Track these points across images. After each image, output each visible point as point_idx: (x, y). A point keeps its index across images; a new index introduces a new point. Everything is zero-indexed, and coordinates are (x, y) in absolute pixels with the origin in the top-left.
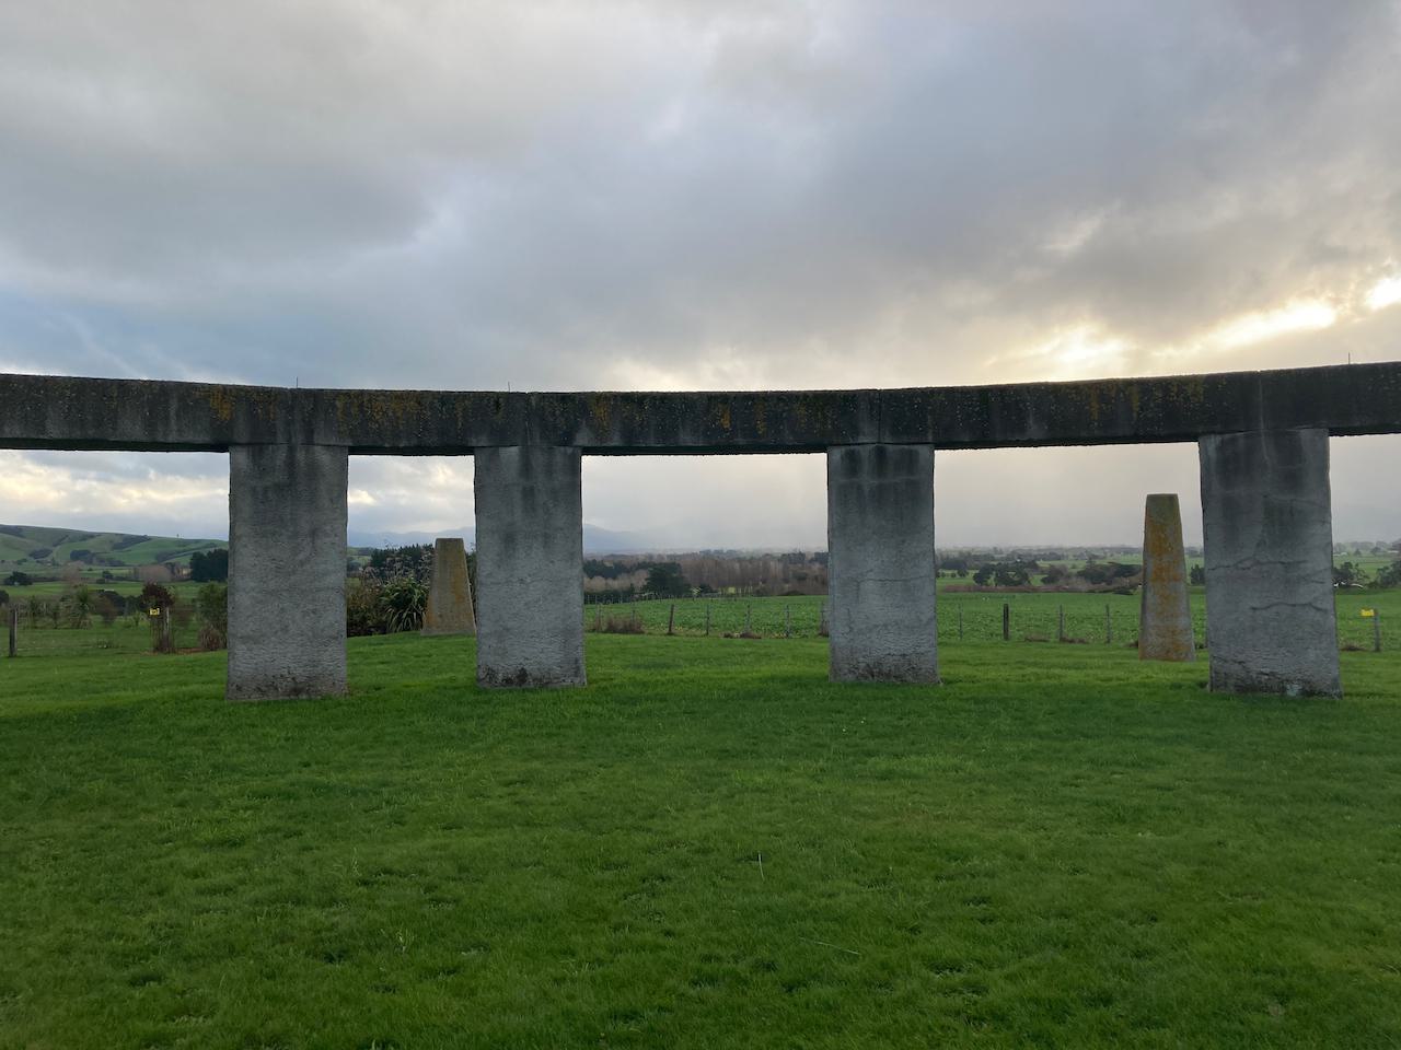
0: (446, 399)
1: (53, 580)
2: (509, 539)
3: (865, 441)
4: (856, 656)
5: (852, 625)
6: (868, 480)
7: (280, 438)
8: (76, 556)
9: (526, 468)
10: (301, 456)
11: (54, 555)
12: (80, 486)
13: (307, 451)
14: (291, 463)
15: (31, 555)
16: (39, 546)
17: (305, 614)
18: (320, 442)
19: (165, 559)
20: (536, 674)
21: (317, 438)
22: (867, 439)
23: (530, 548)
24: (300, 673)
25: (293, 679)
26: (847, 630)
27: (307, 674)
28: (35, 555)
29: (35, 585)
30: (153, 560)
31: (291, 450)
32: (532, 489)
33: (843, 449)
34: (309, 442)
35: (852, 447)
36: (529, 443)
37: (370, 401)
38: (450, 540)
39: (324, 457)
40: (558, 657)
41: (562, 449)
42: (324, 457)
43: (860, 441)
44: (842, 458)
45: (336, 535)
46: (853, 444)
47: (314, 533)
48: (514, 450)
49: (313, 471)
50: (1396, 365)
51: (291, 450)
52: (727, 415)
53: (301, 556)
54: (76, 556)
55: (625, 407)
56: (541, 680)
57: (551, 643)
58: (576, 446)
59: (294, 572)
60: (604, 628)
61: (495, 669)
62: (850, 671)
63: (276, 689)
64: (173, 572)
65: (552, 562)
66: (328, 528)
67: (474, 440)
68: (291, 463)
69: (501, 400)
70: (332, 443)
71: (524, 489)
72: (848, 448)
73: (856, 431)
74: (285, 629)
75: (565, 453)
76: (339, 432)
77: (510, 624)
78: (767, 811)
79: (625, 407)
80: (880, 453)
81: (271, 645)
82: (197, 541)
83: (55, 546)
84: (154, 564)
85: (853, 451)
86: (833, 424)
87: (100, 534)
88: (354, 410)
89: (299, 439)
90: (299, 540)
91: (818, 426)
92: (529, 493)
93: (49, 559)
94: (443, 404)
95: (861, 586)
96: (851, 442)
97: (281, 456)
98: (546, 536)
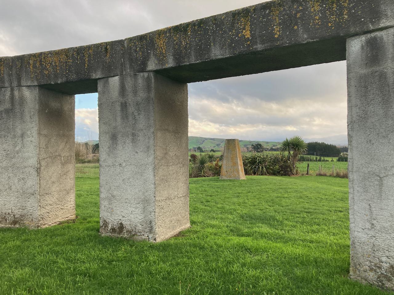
0: (80, 51)
1: (219, 151)
2: (114, 138)
3: (388, 24)
4: (379, 254)
5: (374, 222)
7: (7, 84)
9: (123, 90)
10: (16, 93)
11: (221, 145)
12: (221, 128)
13: (19, 90)
14: (12, 97)
16: (218, 143)
17: (19, 180)
18: (25, 85)
19: (246, 146)
20: (129, 227)
21: (24, 83)
23: (125, 143)
24: (18, 212)
25: (14, 215)
26: (368, 225)
27: (19, 213)
28: (217, 145)
29: (216, 152)
31: (12, 90)
32: (126, 103)
33: (363, 38)
34: (19, 86)
35: (373, 35)
36: (124, 73)
37: (44, 58)
38: (231, 140)
40: (140, 218)
41: (142, 74)
43: (382, 25)
44: (362, 47)
45: (33, 137)
46: (373, 31)
47: (22, 136)
48: (117, 78)
51: (12, 90)
52: (248, 27)
53: (17, 149)
55: (175, 36)
56: (130, 232)
57: (136, 208)
58: (149, 71)
59: (14, 157)
60: (335, 175)
61: (107, 221)
62: (371, 270)
63: (6, 220)
64: (248, 149)
65: (137, 152)
66: (29, 133)
67: (94, 75)
68: (12, 97)
69: (108, 47)
70: (29, 84)
71: (122, 103)
72: (369, 36)
74: (10, 188)
75: (144, 76)
76: (31, 78)
77: (115, 193)
79: (175, 36)
81: (4, 196)
82: (254, 141)
85: (375, 38)
86: (350, 14)
88: (38, 65)
89: (15, 84)
90: (16, 140)
91: (333, 18)
92: (124, 106)
94: (78, 54)
95: (385, 182)
96: (371, 27)
98: (133, 135)
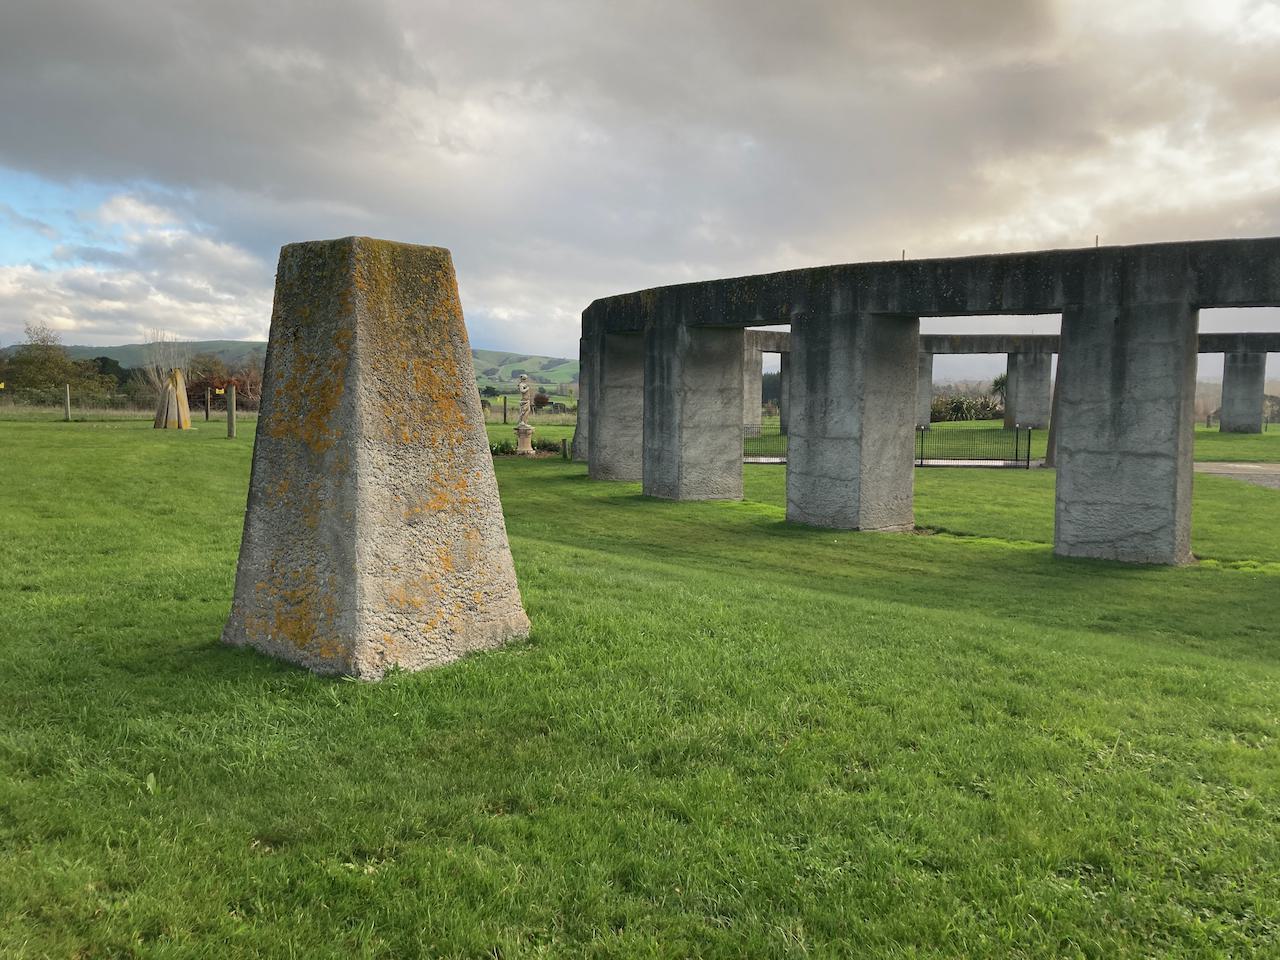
6: (1240, 365)
8: (516, 374)
10: (1038, 356)
15: (484, 373)
16: (489, 366)
22: (1241, 351)
30: (572, 380)
34: (1041, 352)
39: (1045, 357)
42: (1045, 357)
47: (1041, 380)
49: (1042, 361)
50: (1272, 243)
54: (516, 374)
73: (1236, 348)
78: (31, 641)
80: (1245, 355)
83: (500, 366)
84: (571, 382)
87: (531, 357)
89: (1038, 351)
93: (496, 376)
97: (1032, 356)
